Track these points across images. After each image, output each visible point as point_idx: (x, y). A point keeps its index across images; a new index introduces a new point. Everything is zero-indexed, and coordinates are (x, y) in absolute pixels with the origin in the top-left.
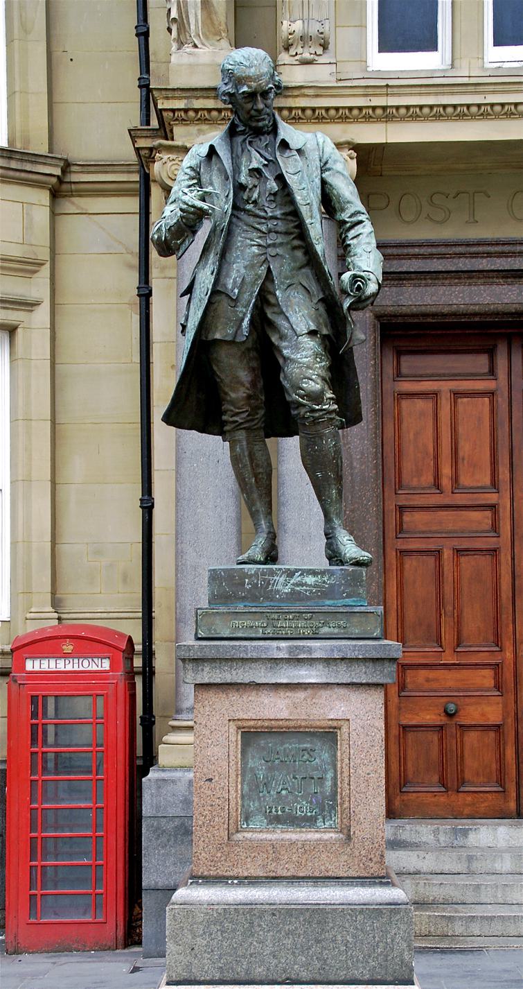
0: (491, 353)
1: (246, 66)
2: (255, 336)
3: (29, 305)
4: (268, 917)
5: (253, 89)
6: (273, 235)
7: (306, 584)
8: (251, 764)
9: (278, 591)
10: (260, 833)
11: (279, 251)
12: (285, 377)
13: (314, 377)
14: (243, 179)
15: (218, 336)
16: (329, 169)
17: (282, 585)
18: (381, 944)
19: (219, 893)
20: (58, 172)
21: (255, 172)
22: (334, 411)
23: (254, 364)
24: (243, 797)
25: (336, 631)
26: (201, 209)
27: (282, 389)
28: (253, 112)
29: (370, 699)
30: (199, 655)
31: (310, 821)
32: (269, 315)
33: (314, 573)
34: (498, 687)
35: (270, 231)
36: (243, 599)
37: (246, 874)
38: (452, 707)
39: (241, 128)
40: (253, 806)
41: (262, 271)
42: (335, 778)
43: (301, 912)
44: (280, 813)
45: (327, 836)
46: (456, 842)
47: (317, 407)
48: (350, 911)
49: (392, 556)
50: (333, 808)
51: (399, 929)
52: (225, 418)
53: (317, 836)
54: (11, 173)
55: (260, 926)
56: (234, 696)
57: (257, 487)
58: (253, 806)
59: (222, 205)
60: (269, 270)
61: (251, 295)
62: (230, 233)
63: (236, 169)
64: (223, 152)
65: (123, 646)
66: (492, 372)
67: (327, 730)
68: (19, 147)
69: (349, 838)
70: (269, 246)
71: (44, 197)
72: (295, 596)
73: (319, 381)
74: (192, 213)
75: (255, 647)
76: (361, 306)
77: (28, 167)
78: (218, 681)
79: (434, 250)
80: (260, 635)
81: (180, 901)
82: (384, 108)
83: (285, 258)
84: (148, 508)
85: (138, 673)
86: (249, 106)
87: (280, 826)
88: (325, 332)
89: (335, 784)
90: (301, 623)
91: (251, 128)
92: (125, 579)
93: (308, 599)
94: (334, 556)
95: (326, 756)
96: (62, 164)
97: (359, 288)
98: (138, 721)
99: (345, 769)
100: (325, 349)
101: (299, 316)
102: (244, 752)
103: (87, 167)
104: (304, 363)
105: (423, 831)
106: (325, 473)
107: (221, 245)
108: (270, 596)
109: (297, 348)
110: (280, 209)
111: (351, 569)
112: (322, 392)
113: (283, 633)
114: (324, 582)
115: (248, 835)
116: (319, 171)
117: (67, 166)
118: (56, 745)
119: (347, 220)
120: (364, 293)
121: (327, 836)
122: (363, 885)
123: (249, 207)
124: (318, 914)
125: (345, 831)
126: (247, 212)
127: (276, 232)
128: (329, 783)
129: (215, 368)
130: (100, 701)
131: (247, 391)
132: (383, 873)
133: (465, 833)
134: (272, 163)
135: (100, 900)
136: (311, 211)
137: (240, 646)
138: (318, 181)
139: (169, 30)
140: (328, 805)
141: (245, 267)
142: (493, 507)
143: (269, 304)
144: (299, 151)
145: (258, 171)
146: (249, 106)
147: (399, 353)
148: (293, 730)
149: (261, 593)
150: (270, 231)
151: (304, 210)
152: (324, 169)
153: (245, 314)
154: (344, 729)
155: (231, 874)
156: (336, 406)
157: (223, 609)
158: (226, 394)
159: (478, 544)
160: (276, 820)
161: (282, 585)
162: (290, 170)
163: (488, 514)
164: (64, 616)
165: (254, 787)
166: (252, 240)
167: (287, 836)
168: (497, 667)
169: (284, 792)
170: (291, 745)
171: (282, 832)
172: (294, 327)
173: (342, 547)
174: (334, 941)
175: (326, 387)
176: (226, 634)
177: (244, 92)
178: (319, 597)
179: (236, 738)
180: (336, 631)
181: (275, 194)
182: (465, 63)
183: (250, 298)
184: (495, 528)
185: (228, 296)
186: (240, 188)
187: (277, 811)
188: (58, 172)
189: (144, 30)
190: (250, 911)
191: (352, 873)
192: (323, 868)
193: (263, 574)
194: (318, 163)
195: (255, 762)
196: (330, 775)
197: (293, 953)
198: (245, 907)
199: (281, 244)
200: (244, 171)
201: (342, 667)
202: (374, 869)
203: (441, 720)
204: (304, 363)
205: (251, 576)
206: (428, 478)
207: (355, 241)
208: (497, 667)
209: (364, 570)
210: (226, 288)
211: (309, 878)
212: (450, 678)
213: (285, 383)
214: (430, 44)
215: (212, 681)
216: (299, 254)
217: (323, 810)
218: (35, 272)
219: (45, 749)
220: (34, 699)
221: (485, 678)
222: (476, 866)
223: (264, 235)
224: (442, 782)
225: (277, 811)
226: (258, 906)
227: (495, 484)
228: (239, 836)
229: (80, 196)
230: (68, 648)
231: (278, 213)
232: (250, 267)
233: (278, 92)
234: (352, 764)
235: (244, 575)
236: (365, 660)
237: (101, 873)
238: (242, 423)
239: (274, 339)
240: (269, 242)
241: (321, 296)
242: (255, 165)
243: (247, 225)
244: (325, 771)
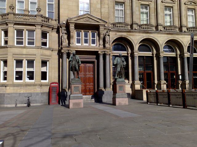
165: (74, 90)
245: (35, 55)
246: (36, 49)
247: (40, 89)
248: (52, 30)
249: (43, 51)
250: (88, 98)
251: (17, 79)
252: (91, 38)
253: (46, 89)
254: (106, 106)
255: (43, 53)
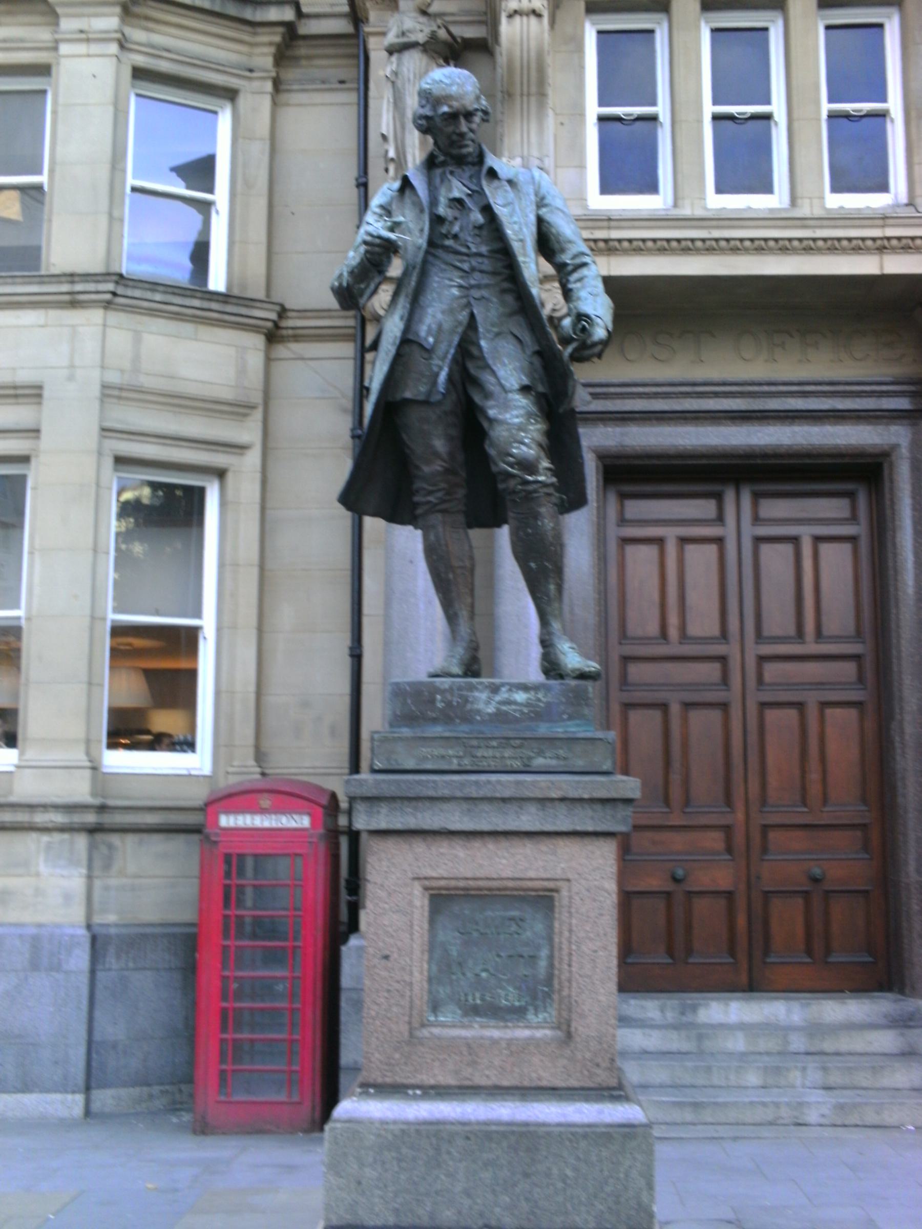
0: (719, 497)
1: (446, 84)
2: (454, 397)
3: (240, 448)
4: (460, 1142)
5: (455, 110)
6: (477, 275)
7: (515, 703)
8: (441, 936)
9: (478, 712)
10: (451, 1027)
11: (485, 293)
12: (492, 445)
13: (526, 441)
14: (442, 210)
15: (408, 395)
16: (545, 206)
17: (484, 702)
18: (611, 1181)
19: (395, 1108)
20: (273, 316)
21: (458, 203)
22: (552, 485)
23: (453, 432)
24: (430, 980)
25: (554, 762)
26: (388, 241)
27: (485, 459)
28: (455, 137)
29: (598, 853)
30: (374, 792)
31: (518, 1013)
32: (473, 371)
33: (525, 688)
34: (729, 850)
35: (473, 269)
36: (435, 721)
37: (432, 1082)
38: (680, 873)
39: (442, 158)
40: (443, 992)
41: (463, 316)
42: (551, 957)
43: (504, 1135)
44: (478, 1002)
45: (539, 1034)
46: (684, 1019)
47: (530, 478)
48: (570, 1136)
49: (615, 708)
50: (548, 995)
51: (635, 1159)
52: (417, 499)
53: (527, 1033)
54: (227, 317)
55: (449, 1153)
56: (419, 847)
57: (455, 583)
58: (443, 992)
59: (413, 235)
60: (472, 316)
61: (450, 346)
62: (424, 274)
63: (434, 202)
64: (419, 182)
65: (325, 801)
66: (720, 519)
67: (541, 893)
68: (236, 292)
69: (569, 1035)
70: (472, 287)
71: (258, 341)
72: (500, 717)
73: (533, 446)
74: (378, 246)
75: (445, 782)
76: (587, 353)
77: (243, 311)
78: (399, 826)
79: (659, 389)
80: (454, 767)
81: (344, 1116)
82: (606, 241)
83: (491, 302)
84: (356, 657)
85: (343, 833)
86: (450, 129)
87: (478, 1019)
88: (541, 388)
89: (551, 966)
90: (508, 753)
91: (453, 157)
92: (333, 732)
93: (517, 720)
94: (552, 667)
95: (539, 927)
96: (278, 308)
97: (584, 329)
98: (343, 883)
99: (565, 946)
100: (541, 409)
101: (508, 371)
102: (432, 921)
103: (304, 313)
104: (515, 424)
105: (650, 1007)
106: (542, 568)
107: (414, 291)
108: (467, 718)
109: (506, 406)
110: (487, 245)
111: (573, 683)
112: (538, 460)
113: (484, 765)
114: (539, 700)
115: (436, 1031)
116: (534, 207)
117: (283, 312)
118: (255, 907)
119: (568, 261)
120: (590, 335)
121: (539, 1034)
122: (587, 1099)
123: (449, 242)
124: (526, 1137)
125: (564, 1027)
126: (447, 249)
127: (482, 272)
128: (543, 963)
129: (405, 437)
130: (299, 862)
131: (444, 464)
132: (613, 1082)
133: (694, 1008)
134: (478, 193)
135: (295, 1077)
136: (524, 248)
137: (428, 781)
138: (532, 218)
139: (387, 170)
140: (541, 991)
141: (443, 312)
142: (723, 659)
143: (471, 356)
144: (510, 182)
145: (459, 201)
146: (450, 129)
147: (623, 497)
148: (498, 893)
149: (457, 712)
150: (473, 269)
151: (516, 246)
152: (541, 203)
153: (441, 368)
154: (564, 893)
155: (412, 1081)
156: (554, 480)
157: (406, 732)
158: (418, 468)
159: (710, 697)
160: (474, 1011)
161: (484, 702)
162: (499, 202)
163: (717, 666)
164: (267, 771)
165: (444, 967)
166: (451, 280)
167: (488, 1033)
168: (727, 829)
169: (484, 975)
170: (495, 913)
171: (482, 1027)
172: (503, 382)
173: (562, 657)
174: (548, 1175)
175: (542, 454)
176: (410, 764)
177: (444, 113)
178: (531, 719)
179: (420, 902)
180: (554, 762)
181: (480, 227)
182: (687, 202)
183: (447, 349)
184: (725, 679)
185: (421, 346)
186: (437, 220)
187: (474, 1000)
188: (273, 316)
189: (363, 180)
190: (435, 1131)
191: (573, 1083)
192: (534, 1075)
193: (460, 688)
194: (533, 198)
195: (448, 935)
196: (544, 953)
197: (494, 1192)
198: (430, 1127)
199: (487, 286)
200: (443, 200)
201: (562, 808)
202: (603, 1077)
203: (670, 887)
204: (515, 424)
205: (445, 691)
206: (653, 628)
207: (578, 285)
208: (727, 829)
209: (589, 686)
210: (418, 336)
211: (517, 1088)
212: (678, 841)
213: (492, 452)
214: (651, 187)
215: (391, 827)
216: (509, 298)
217: (534, 998)
218: (245, 415)
219: (239, 912)
220: (228, 858)
221: (714, 840)
222: (708, 1045)
223: (466, 273)
224: (670, 952)
225: (474, 1000)
226: (448, 1127)
227: (724, 635)
228: (425, 1032)
229: (297, 341)
230: (265, 802)
231: (484, 249)
232: (451, 311)
233: (485, 118)
234: (574, 938)
235: (436, 690)
236: (592, 800)
237: (297, 1048)
238: (436, 505)
239: (477, 398)
240: (473, 282)
241: (537, 348)
242: (456, 194)
243: (447, 263)
244: (538, 948)
245: (32, 393)
246: (54, 314)
247: (75, 881)
248: (282, 57)
249: (137, 339)
250: (798, 1043)
251: (127, 730)
252: (826, 107)
253: (156, 885)
254: (598, 487)
255: (136, 359)
